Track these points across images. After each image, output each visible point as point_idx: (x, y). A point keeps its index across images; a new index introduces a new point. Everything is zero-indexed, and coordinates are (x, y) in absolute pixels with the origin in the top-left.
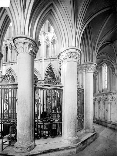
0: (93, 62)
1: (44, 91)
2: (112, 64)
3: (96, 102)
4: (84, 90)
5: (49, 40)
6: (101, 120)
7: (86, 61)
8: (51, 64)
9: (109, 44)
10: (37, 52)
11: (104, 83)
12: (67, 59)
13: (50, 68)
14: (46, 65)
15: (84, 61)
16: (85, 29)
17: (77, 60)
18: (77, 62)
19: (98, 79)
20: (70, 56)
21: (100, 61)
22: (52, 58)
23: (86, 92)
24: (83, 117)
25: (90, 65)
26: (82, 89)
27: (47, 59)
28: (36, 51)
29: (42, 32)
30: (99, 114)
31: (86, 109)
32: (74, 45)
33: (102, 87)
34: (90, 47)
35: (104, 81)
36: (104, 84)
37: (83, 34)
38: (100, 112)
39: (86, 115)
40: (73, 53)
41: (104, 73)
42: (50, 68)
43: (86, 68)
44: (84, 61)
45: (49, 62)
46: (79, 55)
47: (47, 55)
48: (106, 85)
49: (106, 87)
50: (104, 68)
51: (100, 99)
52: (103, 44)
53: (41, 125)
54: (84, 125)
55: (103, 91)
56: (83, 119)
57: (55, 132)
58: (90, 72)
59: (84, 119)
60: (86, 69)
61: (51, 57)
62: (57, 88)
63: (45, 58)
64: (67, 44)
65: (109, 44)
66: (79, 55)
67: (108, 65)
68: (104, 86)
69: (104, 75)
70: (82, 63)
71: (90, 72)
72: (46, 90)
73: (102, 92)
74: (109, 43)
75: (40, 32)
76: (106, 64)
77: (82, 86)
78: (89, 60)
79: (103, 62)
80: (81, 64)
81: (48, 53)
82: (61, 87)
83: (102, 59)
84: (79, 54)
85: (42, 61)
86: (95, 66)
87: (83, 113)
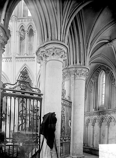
0: (84, 65)
1: (15, 99)
2: (112, 72)
3: (90, 124)
4: (72, 102)
5: (23, 30)
6: (96, 149)
7: (76, 63)
8: (25, 66)
9: (107, 43)
10: (6, 43)
11: (100, 98)
12: (48, 56)
13: (24, 73)
14: (19, 66)
15: (74, 63)
16: (75, 18)
17: (62, 60)
18: (62, 62)
19: (93, 91)
20: (54, 54)
21: (96, 67)
22: (27, 56)
23: (74, 106)
24: (70, 140)
25: (81, 69)
26: (69, 102)
27: (20, 58)
28: (5, 42)
29: (14, 17)
30: (93, 141)
31: (73, 130)
32: (59, 39)
33: (99, 103)
34: (81, 45)
35: (101, 95)
36: (100, 100)
37: (72, 24)
38: (94, 137)
39: (73, 137)
40: (57, 49)
41: (101, 84)
42: (24, 73)
43: (76, 74)
44: (74, 63)
45: (24, 63)
46: (65, 53)
47: (20, 51)
48: (103, 101)
49: (103, 103)
50: (102, 76)
51: (95, 119)
52: (97, 44)
53: (9, 146)
54: (71, 151)
55: (100, 109)
56: (70, 142)
57: (31, 25)
58: (80, 78)
59: (71, 143)
60: (75, 74)
61: (26, 56)
62: (35, 96)
63: (17, 56)
64: (50, 36)
65: (107, 43)
66: (65, 53)
67: (106, 73)
68: (100, 102)
69: (101, 86)
70: (71, 66)
71: (80, 78)
72: (19, 98)
73: (98, 110)
74: (107, 41)
75: (11, 16)
76: (104, 72)
77: (69, 97)
78: (80, 62)
79: (100, 68)
80: (69, 67)
81: (22, 48)
82: (39, 96)
83: (100, 64)
84: (66, 51)
85: (13, 59)
86: (87, 71)
87: (70, 135)
